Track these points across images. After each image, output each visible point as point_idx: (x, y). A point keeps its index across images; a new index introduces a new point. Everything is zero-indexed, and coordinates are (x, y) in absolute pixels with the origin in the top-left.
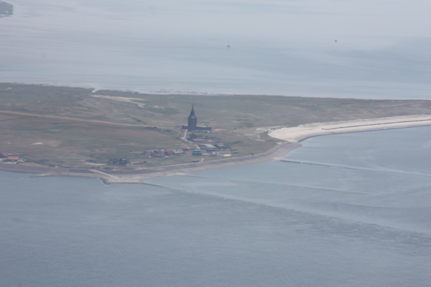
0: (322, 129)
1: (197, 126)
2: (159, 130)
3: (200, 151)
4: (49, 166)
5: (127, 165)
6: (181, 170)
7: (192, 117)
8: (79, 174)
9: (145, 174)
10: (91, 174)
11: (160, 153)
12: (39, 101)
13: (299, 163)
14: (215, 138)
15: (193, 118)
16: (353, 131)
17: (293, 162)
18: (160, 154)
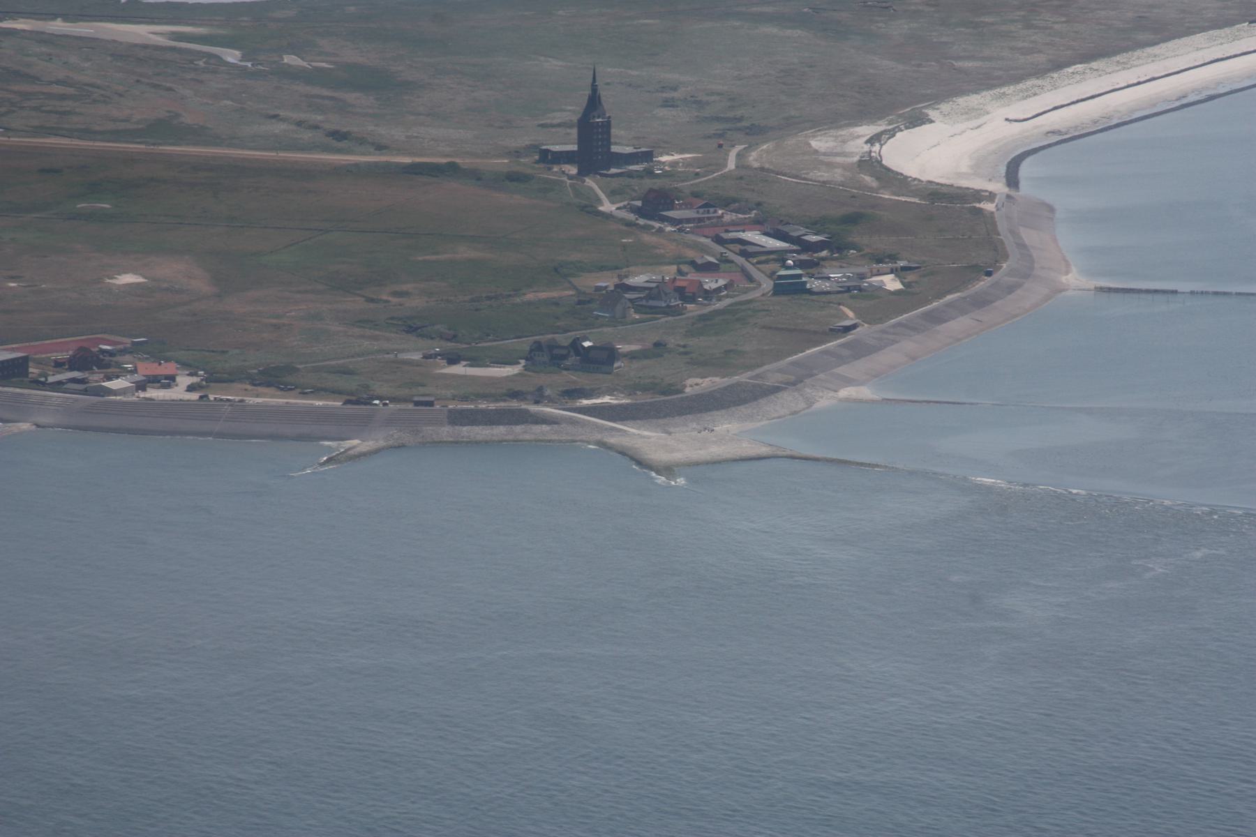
0: (1008, 123)
1: (614, 149)
2: (475, 175)
3: (800, 276)
4: (347, 402)
5: (616, 365)
6: (842, 370)
7: (594, 117)
8: (499, 431)
9: (744, 410)
10: (545, 428)
11: (666, 294)
12: (438, 349)
13: (1175, 292)
14: (735, 200)
15: (598, 122)
16: (1095, 122)
17: (1148, 291)
18: (666, 301)
